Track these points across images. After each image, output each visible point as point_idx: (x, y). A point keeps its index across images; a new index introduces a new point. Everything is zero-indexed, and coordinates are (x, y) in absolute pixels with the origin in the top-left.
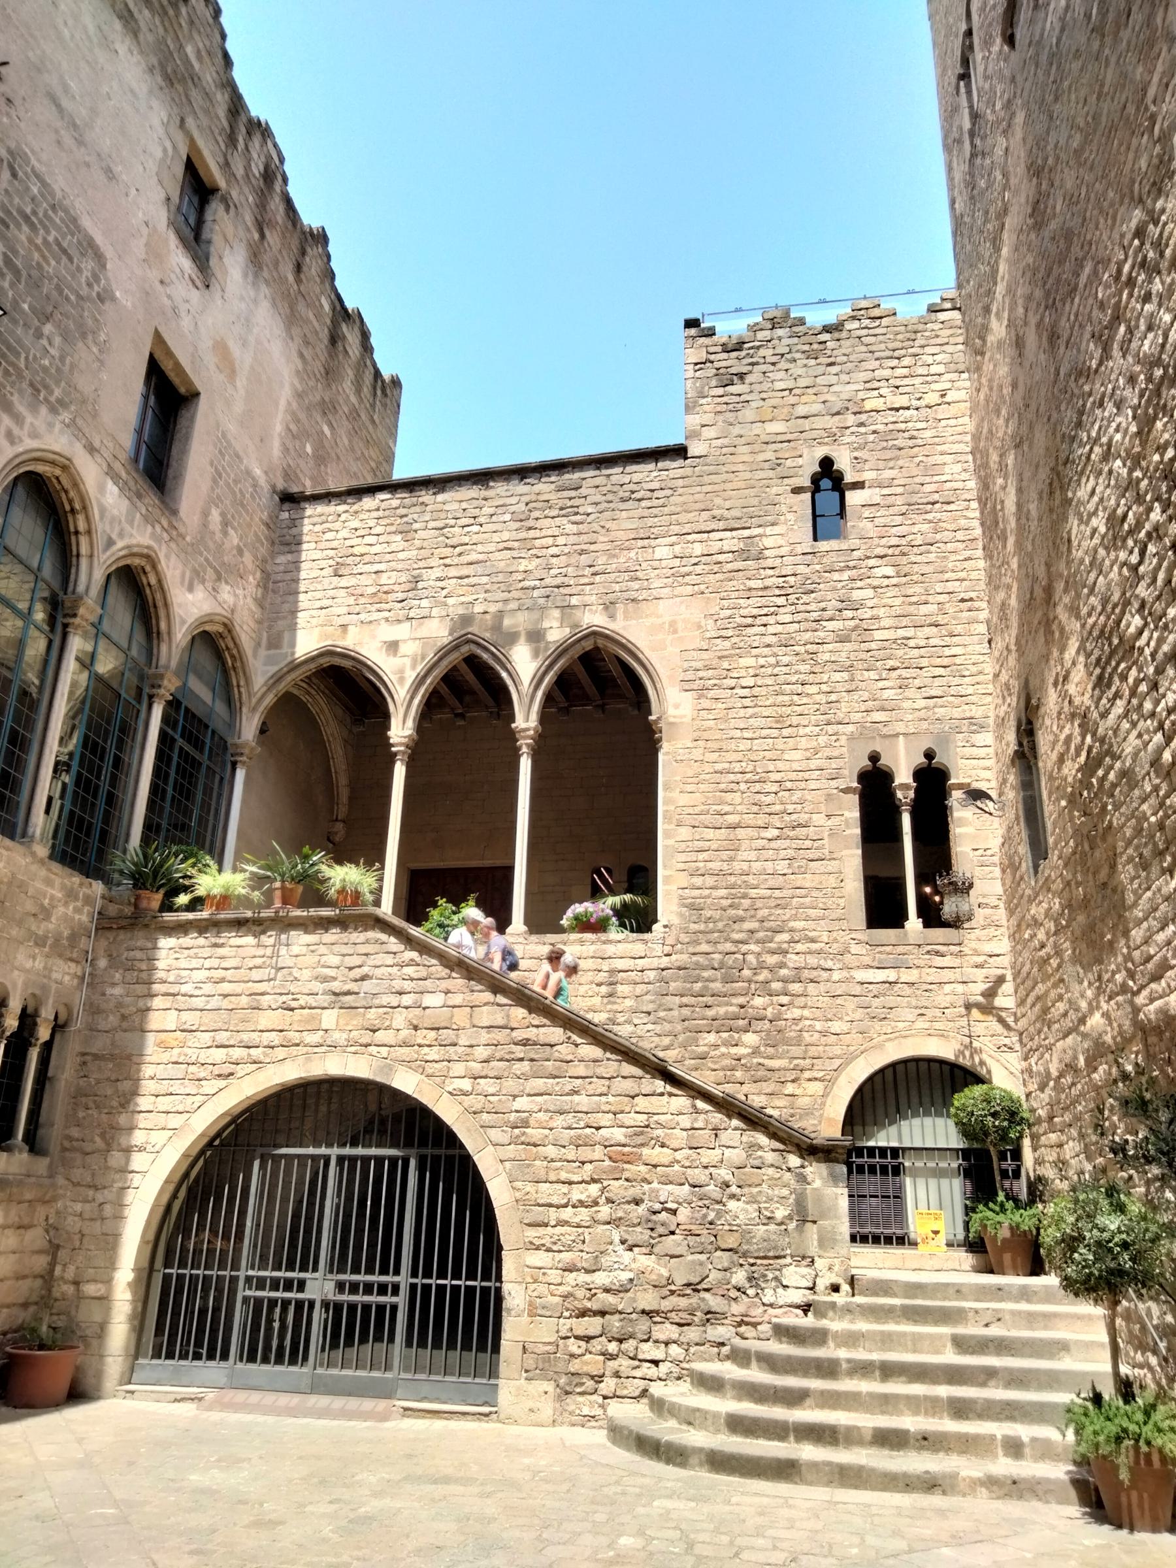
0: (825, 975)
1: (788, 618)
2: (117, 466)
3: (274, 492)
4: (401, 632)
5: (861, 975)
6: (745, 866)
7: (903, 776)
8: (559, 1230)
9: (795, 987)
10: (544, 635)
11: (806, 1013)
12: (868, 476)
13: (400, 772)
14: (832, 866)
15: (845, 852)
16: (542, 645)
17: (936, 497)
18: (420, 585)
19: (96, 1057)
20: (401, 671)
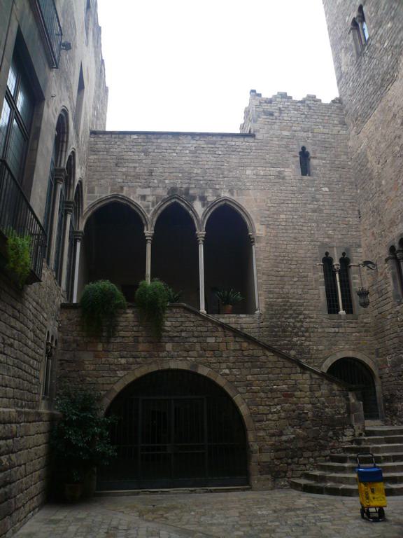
0: (316, 330)
1: (295, 202)
4: (147, 191)
5: (327, 330)
6: (287, 290)
7: (336, 262)
8: (267, 422)
9: (307, 334)
10: (206, 199)
11: (311, 343)
12: (318, 155)
13: (149, 247)
14: (316, 292)
15: (320, 287)
16: (206, 202)
17: (339, 166)
19: (67, 361)
20: (148, 207)
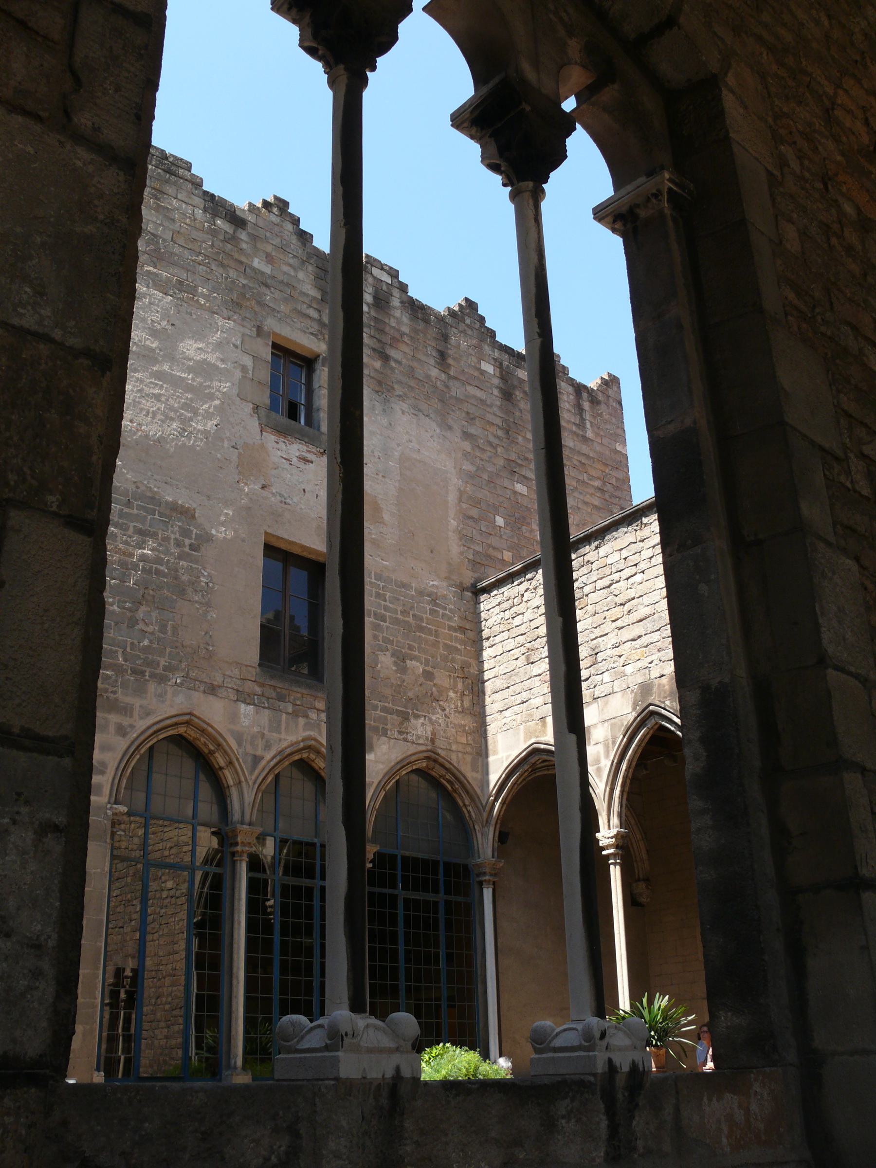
2: (250, 687)
3: (463, 589)
13: (615, 874)
18: (600, 657)
